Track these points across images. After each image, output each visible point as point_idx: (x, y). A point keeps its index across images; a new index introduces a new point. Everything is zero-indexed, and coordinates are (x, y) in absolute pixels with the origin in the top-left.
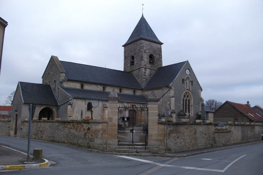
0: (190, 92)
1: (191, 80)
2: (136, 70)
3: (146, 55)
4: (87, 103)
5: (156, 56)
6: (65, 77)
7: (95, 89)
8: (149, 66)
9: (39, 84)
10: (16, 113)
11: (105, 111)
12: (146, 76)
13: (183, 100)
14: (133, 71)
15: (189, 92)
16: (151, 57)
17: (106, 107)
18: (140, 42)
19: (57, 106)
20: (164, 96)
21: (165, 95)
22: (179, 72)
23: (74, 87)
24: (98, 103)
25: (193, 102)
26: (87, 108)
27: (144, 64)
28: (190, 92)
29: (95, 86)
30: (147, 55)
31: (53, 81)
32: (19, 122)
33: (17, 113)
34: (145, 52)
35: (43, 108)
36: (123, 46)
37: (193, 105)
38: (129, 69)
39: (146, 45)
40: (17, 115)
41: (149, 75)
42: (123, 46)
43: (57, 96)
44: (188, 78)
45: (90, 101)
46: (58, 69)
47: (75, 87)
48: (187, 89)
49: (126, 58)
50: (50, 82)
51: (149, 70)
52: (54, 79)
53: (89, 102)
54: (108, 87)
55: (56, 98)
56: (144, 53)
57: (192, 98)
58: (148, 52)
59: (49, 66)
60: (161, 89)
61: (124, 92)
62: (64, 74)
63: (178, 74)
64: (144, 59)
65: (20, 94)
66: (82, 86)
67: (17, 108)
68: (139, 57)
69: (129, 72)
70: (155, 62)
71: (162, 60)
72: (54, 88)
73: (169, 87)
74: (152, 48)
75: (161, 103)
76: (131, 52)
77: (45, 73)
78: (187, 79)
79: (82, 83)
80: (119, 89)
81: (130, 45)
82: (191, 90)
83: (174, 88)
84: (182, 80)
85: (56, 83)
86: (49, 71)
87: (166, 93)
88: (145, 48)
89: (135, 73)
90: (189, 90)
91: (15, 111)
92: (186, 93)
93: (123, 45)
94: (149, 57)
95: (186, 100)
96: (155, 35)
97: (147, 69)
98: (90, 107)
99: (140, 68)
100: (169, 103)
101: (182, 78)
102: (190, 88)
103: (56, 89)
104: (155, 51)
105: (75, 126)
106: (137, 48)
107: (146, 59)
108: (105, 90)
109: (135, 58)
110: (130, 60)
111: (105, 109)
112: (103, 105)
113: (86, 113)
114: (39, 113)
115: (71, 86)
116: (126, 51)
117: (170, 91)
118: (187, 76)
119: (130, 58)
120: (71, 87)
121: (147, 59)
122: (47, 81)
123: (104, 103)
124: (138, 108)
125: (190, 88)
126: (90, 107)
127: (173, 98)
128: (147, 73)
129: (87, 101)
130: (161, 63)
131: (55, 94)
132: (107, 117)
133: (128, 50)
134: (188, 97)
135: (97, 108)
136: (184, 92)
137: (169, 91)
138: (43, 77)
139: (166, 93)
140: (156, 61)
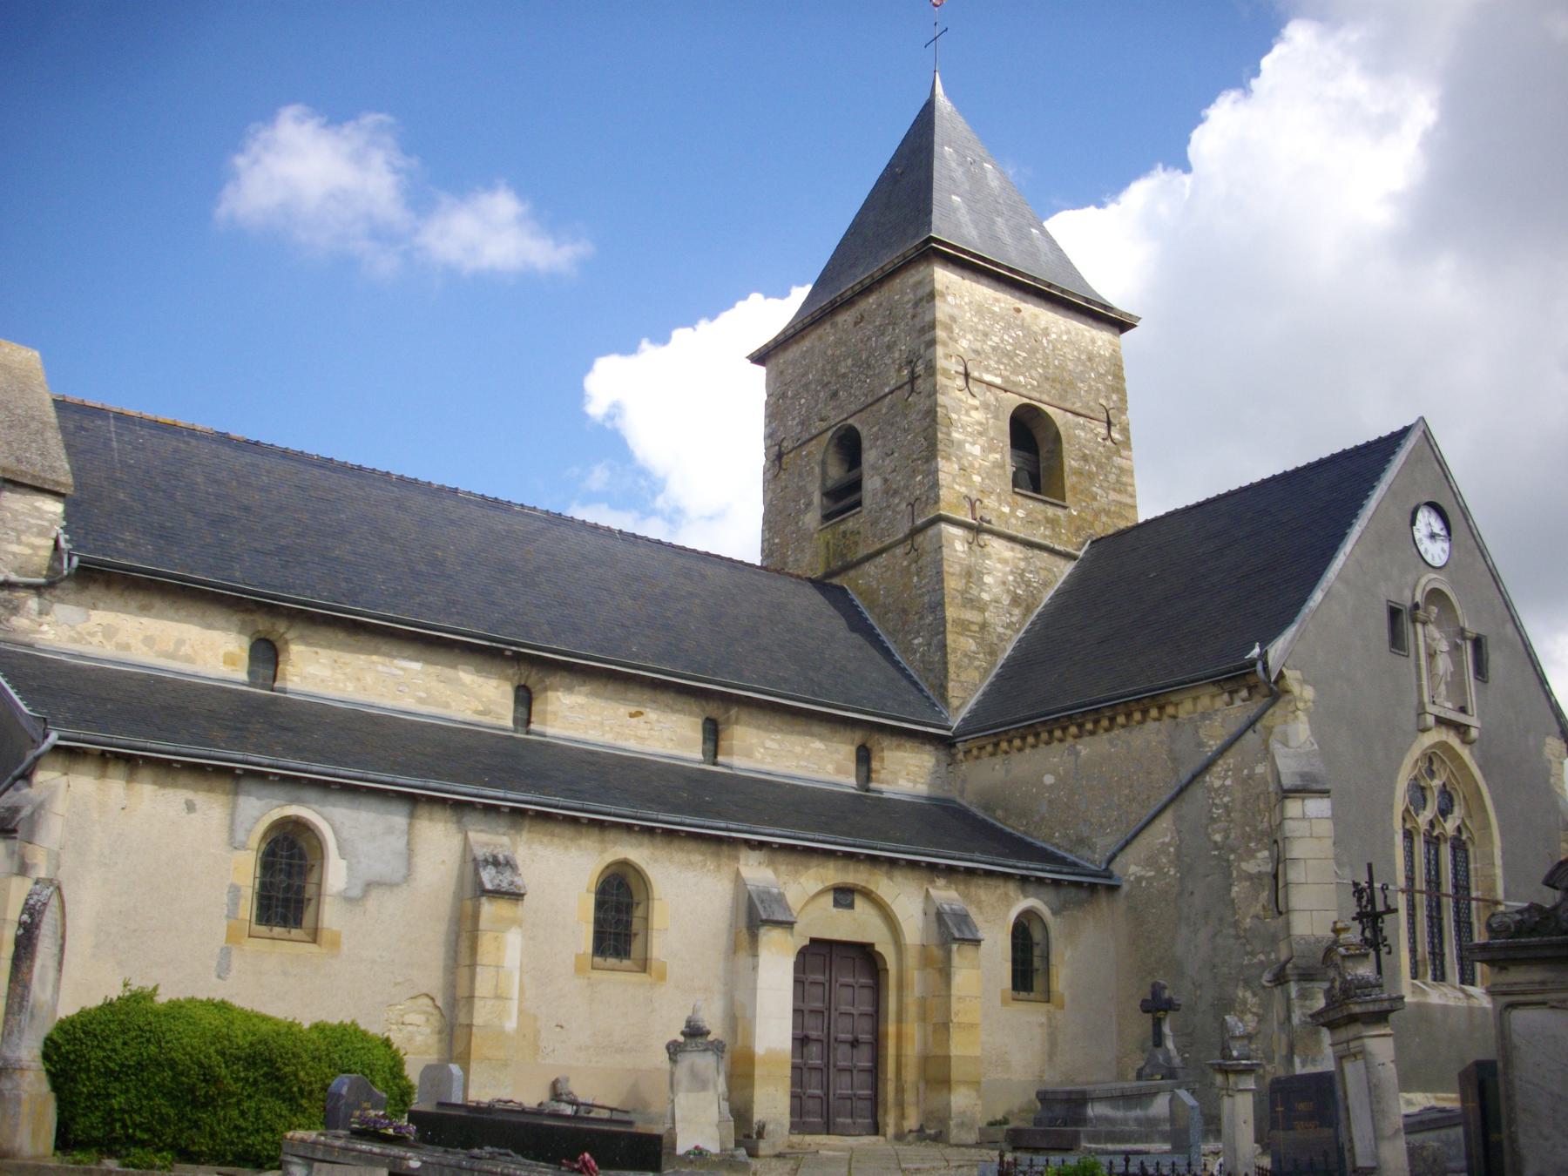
0: (1465, 752)
2: (879, 553)
3: (976, 402)
5: (1078, 436)
6: (57, 542)
7: (421, 701)
8: (1006, 510)
11: (486, 943)
12: (981, 607)
13: (1409, 835)
14: (852, 573)
15: (1456, 757)
16: (1030, 436)
17: (497, 894)
20: (1197, 791)
21: (1213, 779)
24: (399, 843)
25: (1498, 861)
27: (964, 490)
28: (1465, 752)
29: (416, 666)
30: (986, 406)
34: (967, 375)
36: (760, 358)
37: (1500, 894)
38: (807, 558)
39: (980, 311)
41: (1016, 601)
42: (760, 358)
44: (1436, 595)
47: (172, 656)
48: (1441, 721)
51: (1008, 554)
53: (277, 814)
54: (570, 689)
56: (960, 382)
57: (1486, 826)
58: (998, 381)
61: (749, 755)
62: (55, 508)
64: (961, 445)
66: (266, 654)
68: (905, 424)
70: (1070, 480)
73: (1252, 689)
74: (1032, 352)
75: (1159, 870)
76: (835, 395)
78: (1434, 610)
79: (263, 623)
80: (699, 721)
81: (828, 327)
82: (1474, 733)
83: (1308, 693)
84: (1384, 615)
87: (1222, 752)
88: (965, 343)
89: (866, 580)
90: (1461, 729)
92: (1424, 765)
94: (1006, 426)
95: (1433, 842)
98: (286, 887)
99: (916, 531)
100: (1260, 862)
101: (1389, 592)
104: (1062, 383)
107: (983, 440)
109: (865, 444)
110: (824, 473)
111: (488, 909)
112: (470, 867)
113: (236, 963)
115: (127, 647)
117: (1269, 730)
118: (1428, 580)
119: (816, 450)
123: (488, 838)
126: (286, 887)
127: (1318, 807)
128: (988, 579)
129: (261, 811)
130: (1126, 499)
132: (511, 1024)
133: (806, 386)
134: (1444, 812)
135: (385, 906)
137: (1252, 724)
139: (1222, 752)
140: (1079, 473)
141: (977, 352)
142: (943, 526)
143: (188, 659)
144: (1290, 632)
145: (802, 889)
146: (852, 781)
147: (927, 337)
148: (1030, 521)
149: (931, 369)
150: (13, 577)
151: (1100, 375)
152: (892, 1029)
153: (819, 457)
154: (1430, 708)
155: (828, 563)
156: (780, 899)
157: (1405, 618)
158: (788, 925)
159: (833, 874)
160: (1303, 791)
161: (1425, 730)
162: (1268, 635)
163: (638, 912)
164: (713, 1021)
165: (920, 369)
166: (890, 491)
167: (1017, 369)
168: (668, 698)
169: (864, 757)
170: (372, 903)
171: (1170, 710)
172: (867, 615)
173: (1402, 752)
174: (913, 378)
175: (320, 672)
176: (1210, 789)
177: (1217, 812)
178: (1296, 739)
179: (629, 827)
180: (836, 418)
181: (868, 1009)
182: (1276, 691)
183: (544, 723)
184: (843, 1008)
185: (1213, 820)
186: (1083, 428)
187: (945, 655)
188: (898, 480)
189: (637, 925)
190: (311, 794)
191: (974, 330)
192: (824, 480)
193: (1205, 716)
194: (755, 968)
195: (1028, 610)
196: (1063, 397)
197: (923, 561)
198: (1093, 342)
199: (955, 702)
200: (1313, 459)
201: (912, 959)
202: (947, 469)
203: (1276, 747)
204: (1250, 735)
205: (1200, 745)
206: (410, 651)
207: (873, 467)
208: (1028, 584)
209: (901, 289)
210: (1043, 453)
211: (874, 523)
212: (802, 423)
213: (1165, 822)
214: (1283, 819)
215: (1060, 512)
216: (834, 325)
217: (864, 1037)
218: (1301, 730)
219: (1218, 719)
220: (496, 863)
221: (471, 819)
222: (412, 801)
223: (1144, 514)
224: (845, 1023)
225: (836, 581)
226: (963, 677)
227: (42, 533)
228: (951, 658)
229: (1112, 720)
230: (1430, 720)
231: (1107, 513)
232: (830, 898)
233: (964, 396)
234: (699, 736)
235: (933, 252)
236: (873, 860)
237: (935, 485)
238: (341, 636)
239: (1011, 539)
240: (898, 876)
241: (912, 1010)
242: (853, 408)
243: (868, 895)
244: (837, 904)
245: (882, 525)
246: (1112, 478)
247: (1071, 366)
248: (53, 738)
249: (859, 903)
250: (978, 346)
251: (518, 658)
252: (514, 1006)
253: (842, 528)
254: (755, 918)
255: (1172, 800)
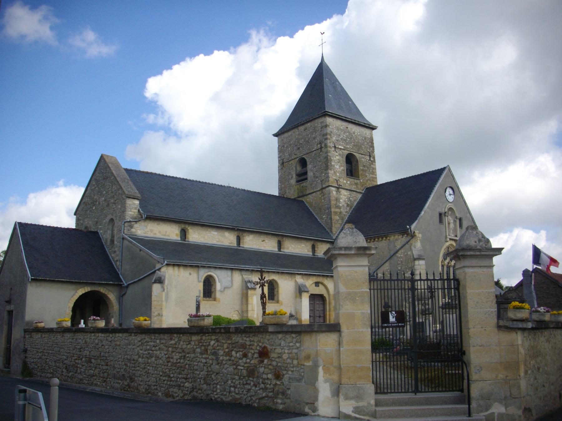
1: (458, 216)
3: (337, 154)
4: (202, 281)
5: (362, 159)
6: (139, 210)
7: (217, 241)
8: (345, 182)
9: (68, 229)
10: (8, 308)
11: (250, 299)
13: (443, 266)
16: (350, 160)
18: (321, 123)
19: (120, 286)
20: (394, 258)
21: (398, 255)
22: (432, 196)
23: (163, 237)
24: (229, 279)
26: (202, 291)
29: (216, 233)
30: (340, 155)
31: (107, 220)
32: (17, 333)
33: (12, 307)
34: (335, 147)
35: (84, 292)
39: (338, 129)
40: (10, 313)
41: (348, 205)
43: (117, 261)
44: (451, 209)
45: (209, 273)
46: (121, 188)
47: (165, 235)
48: (450, 239)
49: (283, 163)
50: (97, 223)
51: (346, 194)
52: (110, 217)
53: (206, 274)
55: (117, 265)
56: (333, 149)
58: (342, 148)
59: (94, 183)
60: (384, 238)
61: (288, 249)
62: (137, 202)
63: (430, 200)
65: (21, 254)
66: (184, 233)
67: (11, 294)
69: (294, 200)
70: (360, 172)
71: (375, 169)
72: (109, 241)
73: (407, 235)
76: (299, 148)
77: (84, 201)
78: (450, 212)
79: (183, 226)
81: (296, 130)
83: (420, 235)
84: (438, 215)
85: (116, 225)
86: (94, 195)
88: (334, 138)
89: (309, 200)
91: (7, 302)
93: (276, 131)
94: (345, 160)
95: (448, 267)
96: (356, 108)
97: (340, 190)
98: (208, 288)
102: (456, 236)
103: (116, 243)
104: (358, 146)
105: (209, 345)
106: (314, 138)
107: (339, 164)
108: (241, 245)
109: (308, 163)
110: (296, 169)
111: (250, 292)
112: (244, 283)
114: (72, 305)
115: (155, 234)
116: (283, 146)
117: (411, 244)
120: (155, 236)
121: (341, 166)
122: (90, 224)
124: (434, 280)
125: (456, 236)
126: (208, 288)
127: (422, 262)
128: (341, 201)
129: (204, 273)
130: (374, 176)
131: (113, 255)
133: (290, 145)
135: (228, 292)
136: (445, 247)
137: (407, 243)
138: (78, 212)
140: (363, 170)
141: (337, 140)
142: (330, 187)
143: (169, 236)
144: (417, 221)
145: (309, 283)
146: (311, 253)
147: (325, 137)
148: (351, 184)
149: (326, 146)
150: (131, 220)
151: (368, 143)
152: (328, 313)
153: (295, 165)
154: (449, 237)
155: (298, 194)
156: (305, 286)
157: (443, 215)
158: (308, 292)
159: (315, 279)
160: (419, 258)
161: (447, 242)
162: (410, 224)
163: (276, 290)
164: (294, 313)
165: (323, 145)
166: (315, 177)
167: (347, 144)
168: (270, 236)
169: (313, 247)
170: (225, 292)
171: (388, 238)
172: (310, 208)
173: (442, 247)
174: (321, 148)
175: (196, 236)
176: (398, 257)
177: (399, 262)
178: (417, 246)
179: (274, 272)
180: (299, 155)
181: (322, 309)
182: (413, 236)
183: (243, 244)
184: (317, 309)
185: (398, 264)
186: (363, 158)
187: (331, 221)
188: (318, 174)
189: (275, 293)
190: (213, 270)
191: (336, 134)
192: (296, 171)
193: (396, 240)
194: (301, 301)
195: (351, 207)
196: (358, 150)
197: (326, 196)
198: (366, 134)
199: (334, 232)
200: (422, 173)
201: (332, 297)
202: (331, 172)
203: (413, 248)
204: (407, 245)
205: (396, 247)
206: (214, 230)
207: (311, 170)
208: (351, 201)
209: (318, 123)
210: (353, 164)
211: (311, 185)
212: (289, 155)
213: (387, 264)
214: (414, 265)
215: (358, 181)
216: (298, 129)
217: (322, 315)
218: (418, 244)
219: (400, 241)
220: (250, 282)
221: (243, 273)
222: (232, 269)
223: (379, 182)
224: (318, 312)
225: (300, 199)
226: (336, 226)
227: (135, 209)
228: (333, 221)
229: (374, 239)
230: (448, 239)
231: (370, 180)
232: (314, 285)
233: (334, 153)
234: (276, 245)
235: (326, 114)
236: (323, 276)
237: (328, 177)
238: (200, 228)
239: (347, 189)
240: (328, 279)
241: (332, 309)
242: (304, 153)
243: (322, 283)
244: (316, 286)
245: (313, 185)
246: (371, 171)
247: (360, 141)
248: (166, 262)
249: (320, 285)
250: (337, 139)
251: (238, 230)
252: (256, 312)
253: (302, 185)
254: (300, 290)
255: (389, 259)
